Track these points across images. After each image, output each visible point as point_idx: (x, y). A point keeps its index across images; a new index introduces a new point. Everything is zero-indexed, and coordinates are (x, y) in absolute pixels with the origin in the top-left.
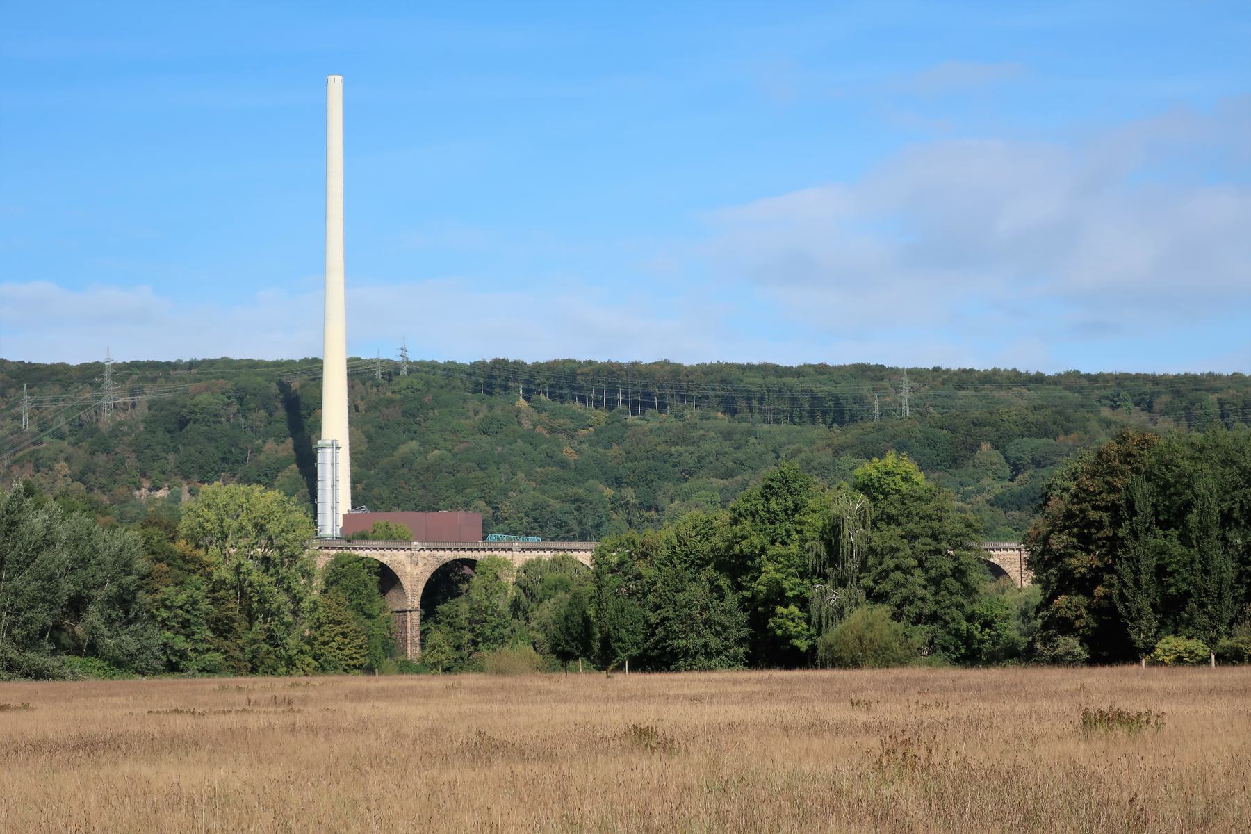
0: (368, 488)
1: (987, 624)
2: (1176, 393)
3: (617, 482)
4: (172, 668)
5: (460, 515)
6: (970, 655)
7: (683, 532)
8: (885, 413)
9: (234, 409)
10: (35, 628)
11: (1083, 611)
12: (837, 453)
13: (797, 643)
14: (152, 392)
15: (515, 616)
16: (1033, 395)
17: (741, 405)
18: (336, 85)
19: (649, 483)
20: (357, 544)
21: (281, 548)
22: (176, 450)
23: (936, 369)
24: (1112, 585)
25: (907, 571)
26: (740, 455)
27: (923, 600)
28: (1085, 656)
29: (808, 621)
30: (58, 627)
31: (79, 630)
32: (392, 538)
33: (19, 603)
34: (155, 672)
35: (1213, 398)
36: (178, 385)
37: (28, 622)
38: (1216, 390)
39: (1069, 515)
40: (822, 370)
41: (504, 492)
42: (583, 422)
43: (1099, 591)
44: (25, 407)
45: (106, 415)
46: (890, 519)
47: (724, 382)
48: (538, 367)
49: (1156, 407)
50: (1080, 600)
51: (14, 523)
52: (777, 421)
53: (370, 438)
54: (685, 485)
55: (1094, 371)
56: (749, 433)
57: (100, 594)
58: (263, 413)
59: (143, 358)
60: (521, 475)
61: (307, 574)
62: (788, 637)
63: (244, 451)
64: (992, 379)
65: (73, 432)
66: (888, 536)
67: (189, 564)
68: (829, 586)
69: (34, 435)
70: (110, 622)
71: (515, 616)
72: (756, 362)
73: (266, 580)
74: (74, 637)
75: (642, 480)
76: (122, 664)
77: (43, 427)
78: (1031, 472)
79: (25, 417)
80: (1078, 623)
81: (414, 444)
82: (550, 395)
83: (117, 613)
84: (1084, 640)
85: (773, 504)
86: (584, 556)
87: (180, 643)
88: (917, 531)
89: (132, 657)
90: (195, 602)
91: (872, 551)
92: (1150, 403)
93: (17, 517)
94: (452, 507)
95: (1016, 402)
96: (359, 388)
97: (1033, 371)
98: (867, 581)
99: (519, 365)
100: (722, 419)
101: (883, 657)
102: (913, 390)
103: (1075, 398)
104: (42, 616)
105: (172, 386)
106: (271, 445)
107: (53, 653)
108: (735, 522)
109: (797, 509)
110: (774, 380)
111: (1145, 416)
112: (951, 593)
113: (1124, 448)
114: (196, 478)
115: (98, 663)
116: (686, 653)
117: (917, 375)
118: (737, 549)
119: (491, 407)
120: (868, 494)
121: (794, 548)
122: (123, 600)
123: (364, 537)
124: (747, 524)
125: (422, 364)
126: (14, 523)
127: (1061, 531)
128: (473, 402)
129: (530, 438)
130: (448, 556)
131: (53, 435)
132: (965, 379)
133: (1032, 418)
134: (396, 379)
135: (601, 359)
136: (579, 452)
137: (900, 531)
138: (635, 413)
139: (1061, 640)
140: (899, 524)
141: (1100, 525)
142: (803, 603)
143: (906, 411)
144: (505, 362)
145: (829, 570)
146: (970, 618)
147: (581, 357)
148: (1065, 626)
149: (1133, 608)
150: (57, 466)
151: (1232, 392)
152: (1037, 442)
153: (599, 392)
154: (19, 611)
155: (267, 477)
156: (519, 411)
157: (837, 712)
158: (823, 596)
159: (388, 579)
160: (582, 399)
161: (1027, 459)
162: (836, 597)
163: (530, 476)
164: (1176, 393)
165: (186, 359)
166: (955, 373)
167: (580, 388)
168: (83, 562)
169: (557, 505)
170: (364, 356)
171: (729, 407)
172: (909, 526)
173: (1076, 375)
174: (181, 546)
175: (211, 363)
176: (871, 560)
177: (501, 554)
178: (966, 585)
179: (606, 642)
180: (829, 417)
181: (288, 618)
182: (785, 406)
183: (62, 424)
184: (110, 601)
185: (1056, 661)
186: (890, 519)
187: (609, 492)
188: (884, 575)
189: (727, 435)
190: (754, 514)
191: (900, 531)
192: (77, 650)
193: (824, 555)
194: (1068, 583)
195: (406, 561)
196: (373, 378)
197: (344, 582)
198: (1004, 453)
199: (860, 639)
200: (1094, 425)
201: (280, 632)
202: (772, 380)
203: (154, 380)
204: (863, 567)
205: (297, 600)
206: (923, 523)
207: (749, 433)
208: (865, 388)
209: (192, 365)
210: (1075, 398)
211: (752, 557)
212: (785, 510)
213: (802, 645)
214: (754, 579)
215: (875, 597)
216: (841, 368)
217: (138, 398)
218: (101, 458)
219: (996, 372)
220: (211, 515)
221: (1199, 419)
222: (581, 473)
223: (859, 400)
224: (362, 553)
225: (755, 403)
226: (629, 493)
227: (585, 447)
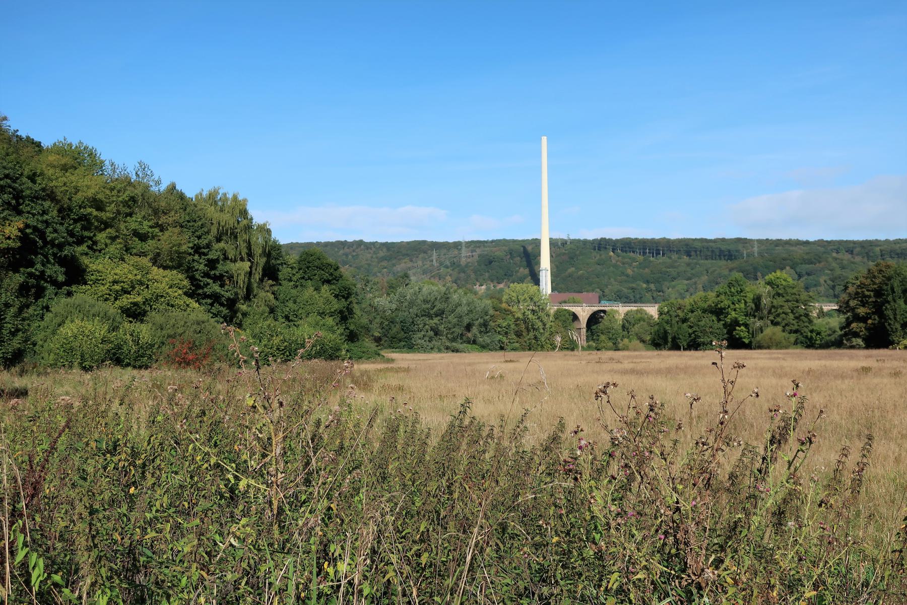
0: (557, 284)
1: (819, 333)
2: (863, 247)
3: (648, 282)
4: (502, 348)
5: (590, 294)
6: (810, 344)
7: (696, 300)
8: (748, 256)
9: (509, 257)
10: (455, 335)
11: (863, 329)
12: (730, 271)
13: (744, 340)
14: (479, 251)
15: (624, 330)
16: (806, 249)
17: (693, 253)
18: (544, 139)
19: (659, 282)
20: (563, 304)
21: (539, 306)
22: (488, 272)
23: (767, 239)
24: (875, 319)
25: (786, 314)
26: (693, 272)
27: (793, 324)
28: (864, 346)
29: (748, 332)
30: (462, 335)
31: (469, 335)
32: (575, 302)
33: (450, 326)
34: (496, 350)
35: (878, 249)
36: (488, 249)
37: (453, 332)
38: (880, 246)
39: (857, 293)
40: (723, 240)
41: (606, 286)
42: (634, 260)
43: (870, 321)
44: (434, 257)
45: (463, 260)
46: (779, 295)
47: (687, 245)
48: (617, 240)
49: (854, 252)
50: (861, 325)
51: (448, 298)
52: (707, 259)
53: (557, 267)
54: (673, 283)
55: (829, 239)
56: (696, 264)
57: (477, 323)
58: (519, 258)
59: (475, 239)
60: (612, 279)
61: (548, 315)
62: (741, 338)
63: (512, 272)
64: (789, 243)
65: (451, 266)
66: (779, 301)
67: (507, 312)
68: (756, 319)
69: (438, 267)
70: (481, 332)
71: (624, 330)
72: (698, 237)
73: (534, 317)
74: (468, 338)
75: (657, 281)
76: (484, 347)
77: (441, 264)
78: (806, 277)
79: (434, 261)
80: (861, 333)
81: (573, 269)
82: (622, 251)
83: (483, 329)
84: (864, 340)
85: (733, 290)
86: (653, 311)
87: (505, 340)
88: (790, 299)
89: (488, 345)
90: (510, 325)
91: (773, 307)
92: (852, 251)
93: (449, 296)
94: (587, 291)
95: (800, 251)
96: (553, 249)
97: (805, 240)
98: (771, 318)
99: (610, 240)
100: (686, 258)
101: (778, 345)
102: (758, 247)
103: (822, 249)
104: (458, 331)
105: (486, 249)
106: (522, 269)
107: (461, 343)
108: (718, 296)
109: (741, 291)
110: (706, 244)
111: (850, 256)
112: (804, 322)
113: (879, 268)
114: (495, 282)
115: (477, 347)
116: (704, 344)
117: (760, 241)
118: (719, 306)
119: (600, 255)
120: (771, 286)
121: (743, 306)
122: (485, 325)
123: (565, 302)
124: (723, 297)
125: (575, 240)
126: (448, 298)
127: (854, 299)
128: (594, 253)
129: (615, 266)
130: (596, 309)
131: (445, 267)
132: (778, 243)
133: (806, 257)
134: (566, 246)
135: (640, 237)
136: (633, 271)
137: (784, 299)
138: (653, 257)
139: (854, 339)
140: (783, 297)
141: (869, 297)
142: (746, 325)
143: (756, 255)
144: (605, 239)
145: (756, 314)
146: (812, 331)
147: (633, 237)
148: (856, 335)
149: (894, 327)
150: (447, 278)
151: (886, 246)
152: (808, 266)
153: (640, 249)
154: (450, 329)
155: (521, 280)
156: (611, 257)
157: (772, 363)
158: (754, 323)
159: (575, 317)
160: (633, 252)
161: (804, 273)
162: (758, 324)
163: (616, 280)
164: (863, 247)
165: (490, 239)
166: (775, 241)
167: (633, 248)
168: (471, 311)
169: (625, 290)
170: (554, 237)
171: (689, 254)
172: (788, 298)
173: (822, 240)
174: (504, 305)
175: (500, 241)
176: (773, 310)
177: (615, 308)
178: (809, 319)
179: (674, 339)
180: (726, 258)
181: (542, 331)
182: (709, 254)
183: (448, 263)
184: (480, 325)
185: (852, 347)
186: (779, 295)
187: (645, 286)
188: (778, 315)
189: (688, 265)
190: (725, 293)
191: (784, 299)
192: (469, 342)
193: (754, 308)
194: (857, 318)
195: (581, 311)
196: (557, 245)
197: (561, 318)
198: (795, 270)
199: (771, 339)
200: (830, 259)
201: (539, 336)
202: (705, 244)
203: (479, 247)
204: (770, 312)
205: (544, 325)
206: (793, 296)
207: (696, 264)
208: (740, 247)
209: (493, 241)
210: (822, 249)
211: (724, 309)
212: (737, 292)
213: (746, 341)
214: (726, 317)
215: (775, 324)
216: (731, 239)
217: (474, 253)
218: (462, 275)
219: (790, 240)
220: (514, 294)
221: (872, 257)
222: (634, 279)
223: (737, 251)
224: (567, 308)
225: (698, 252)
226: (652, 286)
227: (635, 269)
